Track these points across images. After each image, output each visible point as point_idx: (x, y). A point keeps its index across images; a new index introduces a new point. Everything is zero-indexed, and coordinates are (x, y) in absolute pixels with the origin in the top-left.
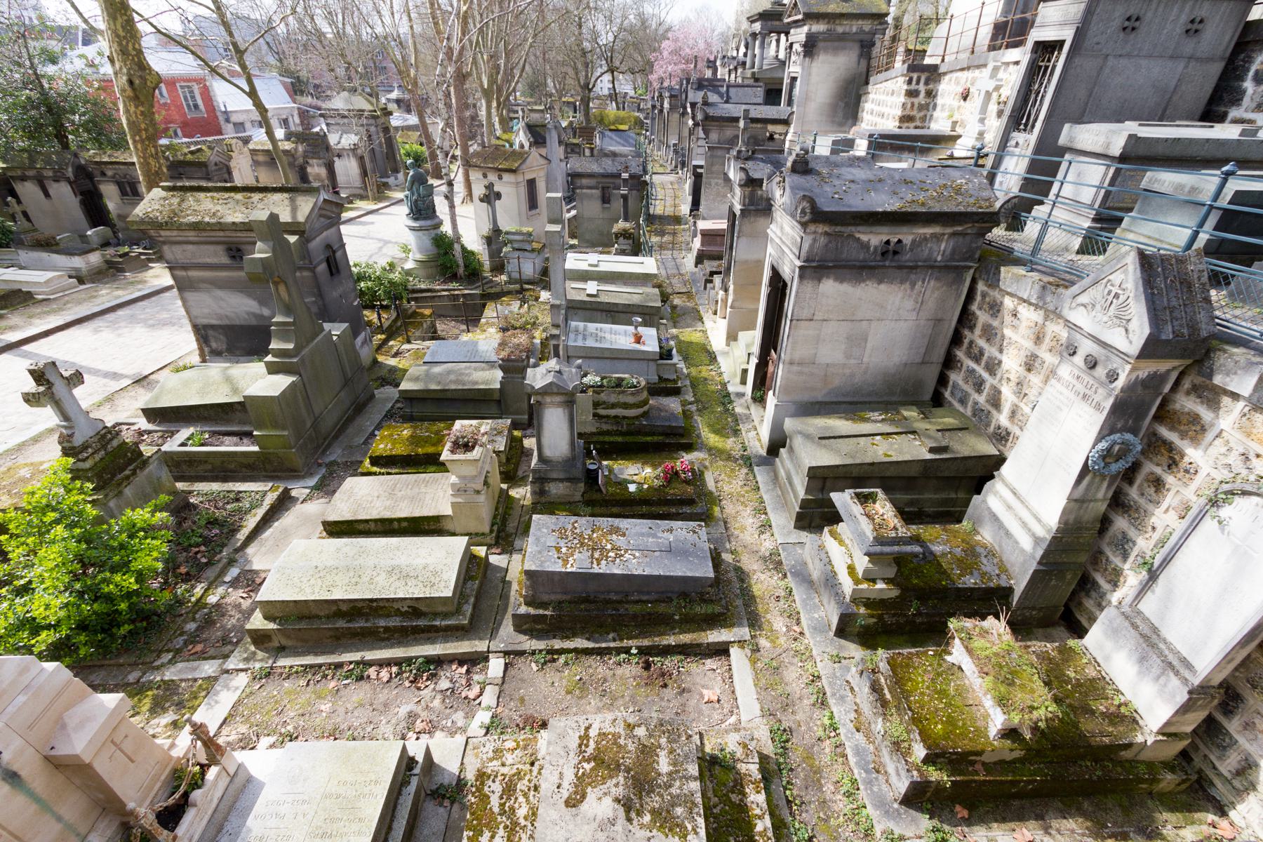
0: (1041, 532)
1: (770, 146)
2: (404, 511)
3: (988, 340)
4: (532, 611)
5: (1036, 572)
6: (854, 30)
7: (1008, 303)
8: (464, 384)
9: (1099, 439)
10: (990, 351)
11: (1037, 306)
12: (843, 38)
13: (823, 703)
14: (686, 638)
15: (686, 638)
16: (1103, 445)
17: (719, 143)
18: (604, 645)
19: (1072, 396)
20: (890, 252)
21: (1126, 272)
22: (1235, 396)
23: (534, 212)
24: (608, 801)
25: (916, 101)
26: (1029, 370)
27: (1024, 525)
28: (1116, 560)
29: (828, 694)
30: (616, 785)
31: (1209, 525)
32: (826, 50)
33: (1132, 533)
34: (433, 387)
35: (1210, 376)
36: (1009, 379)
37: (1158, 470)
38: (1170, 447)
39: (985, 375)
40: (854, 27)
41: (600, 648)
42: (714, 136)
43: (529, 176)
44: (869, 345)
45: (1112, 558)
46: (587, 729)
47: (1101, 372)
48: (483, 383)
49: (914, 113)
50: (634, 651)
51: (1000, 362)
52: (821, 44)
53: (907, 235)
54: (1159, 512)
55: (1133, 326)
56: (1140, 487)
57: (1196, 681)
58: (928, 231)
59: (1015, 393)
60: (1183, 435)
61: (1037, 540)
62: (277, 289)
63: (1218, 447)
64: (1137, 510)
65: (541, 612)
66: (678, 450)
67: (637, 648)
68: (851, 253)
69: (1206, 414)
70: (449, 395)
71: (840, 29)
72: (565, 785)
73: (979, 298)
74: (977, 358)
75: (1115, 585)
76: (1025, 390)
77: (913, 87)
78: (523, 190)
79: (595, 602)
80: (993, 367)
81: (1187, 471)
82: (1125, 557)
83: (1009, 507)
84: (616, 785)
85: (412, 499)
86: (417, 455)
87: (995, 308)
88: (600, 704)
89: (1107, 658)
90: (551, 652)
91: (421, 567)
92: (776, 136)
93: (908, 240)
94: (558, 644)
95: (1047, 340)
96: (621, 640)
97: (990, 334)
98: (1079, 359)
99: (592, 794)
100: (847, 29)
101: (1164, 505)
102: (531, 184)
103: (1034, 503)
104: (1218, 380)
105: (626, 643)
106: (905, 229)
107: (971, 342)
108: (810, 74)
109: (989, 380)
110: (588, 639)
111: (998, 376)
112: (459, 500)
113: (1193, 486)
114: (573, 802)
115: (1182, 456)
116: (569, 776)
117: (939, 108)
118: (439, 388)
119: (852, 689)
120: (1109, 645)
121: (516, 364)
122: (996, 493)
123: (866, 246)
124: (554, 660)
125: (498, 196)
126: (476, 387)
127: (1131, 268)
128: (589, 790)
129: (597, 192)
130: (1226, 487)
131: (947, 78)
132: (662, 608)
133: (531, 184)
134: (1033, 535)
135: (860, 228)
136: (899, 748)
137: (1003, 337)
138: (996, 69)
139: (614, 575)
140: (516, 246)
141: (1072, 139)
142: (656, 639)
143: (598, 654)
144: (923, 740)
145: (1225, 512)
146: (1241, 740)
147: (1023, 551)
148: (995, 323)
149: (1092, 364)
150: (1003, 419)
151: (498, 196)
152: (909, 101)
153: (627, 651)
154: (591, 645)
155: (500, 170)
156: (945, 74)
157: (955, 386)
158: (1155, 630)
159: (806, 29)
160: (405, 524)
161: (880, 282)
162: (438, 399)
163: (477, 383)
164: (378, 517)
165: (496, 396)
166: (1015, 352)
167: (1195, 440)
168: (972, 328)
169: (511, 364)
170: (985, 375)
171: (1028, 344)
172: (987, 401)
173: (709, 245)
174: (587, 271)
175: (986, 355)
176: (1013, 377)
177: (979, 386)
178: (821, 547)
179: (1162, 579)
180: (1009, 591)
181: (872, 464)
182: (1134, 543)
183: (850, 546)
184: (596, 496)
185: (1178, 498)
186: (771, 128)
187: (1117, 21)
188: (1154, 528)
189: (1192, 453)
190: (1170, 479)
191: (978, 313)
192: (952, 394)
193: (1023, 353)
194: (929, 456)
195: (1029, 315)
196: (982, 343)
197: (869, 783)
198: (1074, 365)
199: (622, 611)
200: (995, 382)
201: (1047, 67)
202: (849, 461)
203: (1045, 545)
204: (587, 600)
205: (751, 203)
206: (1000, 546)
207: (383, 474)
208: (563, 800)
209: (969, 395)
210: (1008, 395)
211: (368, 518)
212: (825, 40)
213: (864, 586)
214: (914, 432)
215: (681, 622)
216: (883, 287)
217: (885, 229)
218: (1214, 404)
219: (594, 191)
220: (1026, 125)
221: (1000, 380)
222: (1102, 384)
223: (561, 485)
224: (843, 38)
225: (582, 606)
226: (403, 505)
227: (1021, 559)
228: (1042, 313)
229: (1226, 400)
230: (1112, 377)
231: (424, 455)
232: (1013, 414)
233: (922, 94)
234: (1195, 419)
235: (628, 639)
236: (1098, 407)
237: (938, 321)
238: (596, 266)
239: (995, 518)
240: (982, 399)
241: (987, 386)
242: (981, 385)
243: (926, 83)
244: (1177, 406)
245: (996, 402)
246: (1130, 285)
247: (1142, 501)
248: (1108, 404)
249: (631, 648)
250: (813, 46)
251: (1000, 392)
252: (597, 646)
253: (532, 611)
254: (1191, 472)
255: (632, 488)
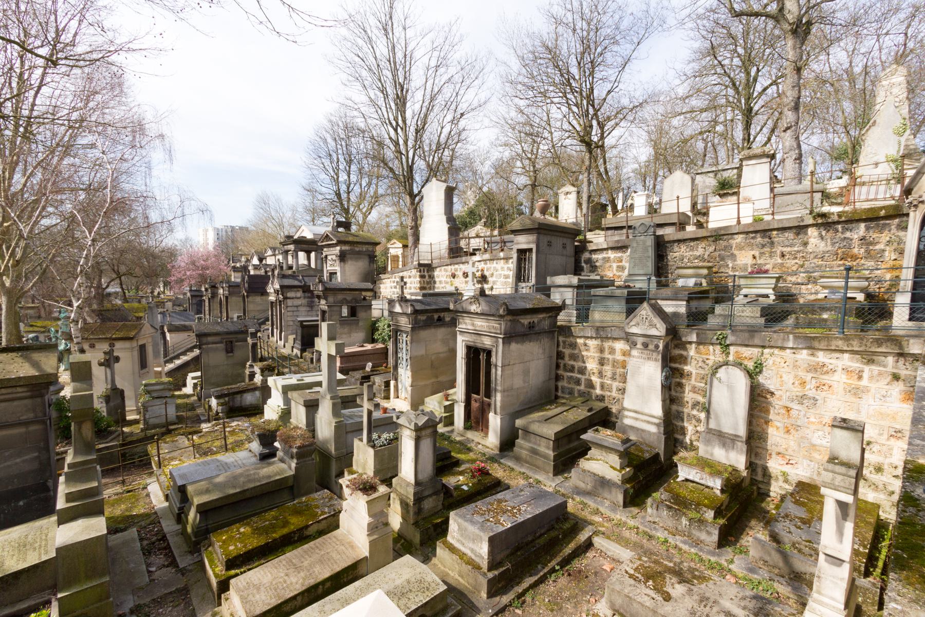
0: (657, 421)
1: (364, 303)
2: (324, 573)
3: (575, 360)
4: (496, 573)
5: (665, 438)
6: (364, 249)
7: (580, 341)
8: (259, 481)
9: (662, 372)
10: (577, 364)
11: (596, 338)
12: (359, 253)
13: (651, 537)
14: (572, 546)
15: (572, 546)
16: (664, 374)
17: (334, 303)
18: (542, 574)
19: (642, 360)
20: (531, 326)
21: (646, 310)
22: (690, 343)
23: (144, 371)
24: (677, 586)
25: (425, 280)
26: (603, 365)
27: (648, 422)
28: (680, 424)
29: (649, 531)
30: (671, 579)
31: (715, 382)
32: (351, 259)
33: (680, 409)
34: (232, 491)
35: (680, 339)
36: (593, 373)
37: (678, 380)
38: (677, 369)
39: (579, 376)
40: (364, 248)
41: (541, 577)
42: (331, 299)
43: (141, 343)
44: (531, 374)
45: (677, 424)
46: (627, 572)
47: (651, 347)
48: (276, 475)
49: (425, 285)
50: (557, 568)
51: (586, 367)
52: (348, 256)
53: (535, 318)
54: (686, 395)
55: (658, 326)
56: (675, 390)
57: (744, 440)
58: (541, 316)
59: (599, 378)
60: (680, 363)
61: (658, 425)
62: (80, 428)
63: (694, 363)
64: (678, 399)
65: (501, 570)
66: (452, 468)
67: (558, 564)
68: (520, 329)
69: (684, 353)
70: (248, 495)
71: (357, 249)
72: (654, 596)
73: (561, 344)
74: (572, 369)
75: (684, 434)
76: (604, 374)
77: (422, 273)
78: (136, 353)
79: (522, 548)
80: (582, 371)
81: (688, 375)
82: (683, 420)
83: (637, 419)
84: (671, 579)
85: (321, 561)
86: (275, 540)
87: (574, 346)
88: (573, 605)
89: (712, 455)
90: (520, 596)
91: (405, 583)
92: (367, 298)
93: (536, 320)
94: (519, 589)
95: (606, 350)
96: (546, 565)
97: (574, 357)
98: (639, 346)
99: (668, 589)
100: (361, 249)
101: (687, 391)
102: (142, 348)
103: (646, 411)
104: (684, 339)
105: (550, 565)
106: (535, 316)
107: (565, 365)
108: (345, 271)
109: (583, 378)
110: (531, 576)
111: (587, 374)
112: (375, 537)
113: (693, 379)
114: (667, 598)
115: (683, 370)
116: (652, 593)
117: (438, 283)
118: (238, 490)
119: (654, 523)
120: (709, 448)
121: (309, 448)
122: (627, 417)
123: (523, 325)
124: (524, 602)
125: (117, 359)
126: (273, 479)
127: (647, 308)
128: (665, 589)
129: (221, 346)
130: (714, 367)
131: (438, 269)
132: (553, 534)
133: (142, 348)
134: (655, 424)
135: (522, 317)
136: (701, 522)
137: (583, 356)
138: (474, 264)
139: (529, 519)
140: (155, 395)
141: (553, 282)
142: (561, 554)
143: (541, 583)
144: (708, 508)
145: (718, 375)
146: (757, 462)
147: (654, 433)
148: (576, 352)
149: (646, 346)
150: (598, 391)
151: (117, 359)
152: (422, 280)
153: (553, 571)
154: (536, 578)
155: (111, 339)
156: (436, 268)
157: (563, 388)
158: (720, 432)
159: (338, 248)
160: (328, 585)
161: (530, 341)
162: (232, 503)
163: (270, 477)
164: (304, 588)
165: (290, 483)
166: (592, 360)
167: (685, 363)
168: (563, 358)
169: (305, 449)
170: (579, 376)
171: (597, 355)
172: (586, 387)
173: (346, 363)
174: (298, 384)
175: (576, 367)
176: (595, 371)
177: (578, 382)
178: (584, 471)
179: (712, 412)
180: (657, 455)
181: (574, 424)
182: (683, 412)
183: (603, 458)
184: (451, 500)
185: (690, 386)
186: (364, 293)
187: (546, 243)
188: (687, 402)
189: (687, 368)
190: (684, 381)
191: (564, 350)
192: (563, 392)
193: (596, 359)
194: (589, 414)
195: (592, 343)
196: (572, 363)
197: (701, 550)
198: (638, 349)
199: (537, 546)
200: (587, 377)
201: (525, 259)
202: (566, 426)
203: (662, 425)
204: (518, 549)
205: (416, 324)
206: (642, 438)
207: (245, 572)
208: (663, 601)
209: (574, 388)
210: (595, 379)
211: (292, 594)
212: (350, 254)
213: (623, 472)
214: (574, 407)
215: (565, 536)
216: (531, 344)
217: (529, 316)
218: (686, 349)
219: (218, 345)
220: (524, 280)
221: (589, 375)
222: (653, 351)
223: (431, 500)
224: (359, 253)
225: (519, 553)
226: (317, 569)
227: (656, 437)
228: (599, 340)
229: (688, 346)
230: (657, 347)
231: (280, 538)
232: (602, 387)
233: (427, 277)
234: (681, 356)
235: (549, 562)
236: (656, 360)
237: (551, 357)
238: (303, 380)
239: (632, 427)
240: (582, 387)
241: (583, 380)
242: (579, 381)
243: (428, 272)
244: (673, 354)
245: (590, 385)
246: (650, 313)
247: (678, 394)
248: (660, 357)
249: (554, 567)
250: (345, 257)
251: (591, 380)
252: (539, 576)
253: (496, 573)
254: (689, 375)
255: (465, 488)
